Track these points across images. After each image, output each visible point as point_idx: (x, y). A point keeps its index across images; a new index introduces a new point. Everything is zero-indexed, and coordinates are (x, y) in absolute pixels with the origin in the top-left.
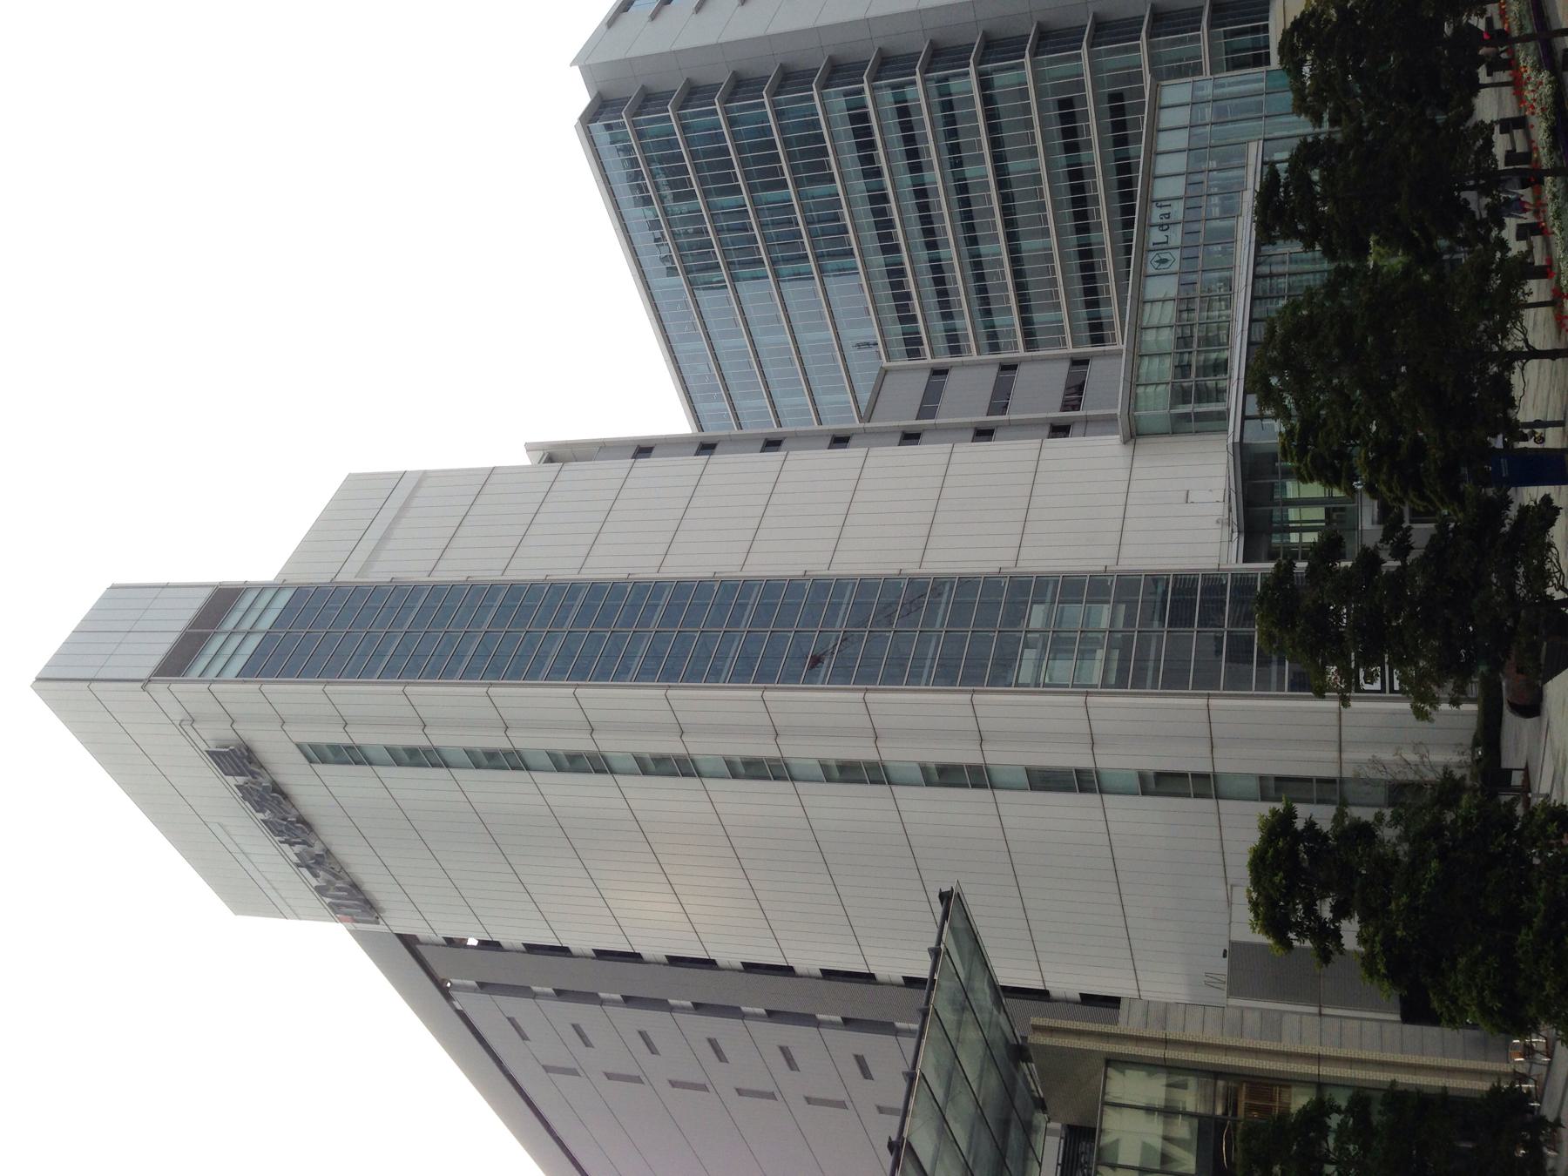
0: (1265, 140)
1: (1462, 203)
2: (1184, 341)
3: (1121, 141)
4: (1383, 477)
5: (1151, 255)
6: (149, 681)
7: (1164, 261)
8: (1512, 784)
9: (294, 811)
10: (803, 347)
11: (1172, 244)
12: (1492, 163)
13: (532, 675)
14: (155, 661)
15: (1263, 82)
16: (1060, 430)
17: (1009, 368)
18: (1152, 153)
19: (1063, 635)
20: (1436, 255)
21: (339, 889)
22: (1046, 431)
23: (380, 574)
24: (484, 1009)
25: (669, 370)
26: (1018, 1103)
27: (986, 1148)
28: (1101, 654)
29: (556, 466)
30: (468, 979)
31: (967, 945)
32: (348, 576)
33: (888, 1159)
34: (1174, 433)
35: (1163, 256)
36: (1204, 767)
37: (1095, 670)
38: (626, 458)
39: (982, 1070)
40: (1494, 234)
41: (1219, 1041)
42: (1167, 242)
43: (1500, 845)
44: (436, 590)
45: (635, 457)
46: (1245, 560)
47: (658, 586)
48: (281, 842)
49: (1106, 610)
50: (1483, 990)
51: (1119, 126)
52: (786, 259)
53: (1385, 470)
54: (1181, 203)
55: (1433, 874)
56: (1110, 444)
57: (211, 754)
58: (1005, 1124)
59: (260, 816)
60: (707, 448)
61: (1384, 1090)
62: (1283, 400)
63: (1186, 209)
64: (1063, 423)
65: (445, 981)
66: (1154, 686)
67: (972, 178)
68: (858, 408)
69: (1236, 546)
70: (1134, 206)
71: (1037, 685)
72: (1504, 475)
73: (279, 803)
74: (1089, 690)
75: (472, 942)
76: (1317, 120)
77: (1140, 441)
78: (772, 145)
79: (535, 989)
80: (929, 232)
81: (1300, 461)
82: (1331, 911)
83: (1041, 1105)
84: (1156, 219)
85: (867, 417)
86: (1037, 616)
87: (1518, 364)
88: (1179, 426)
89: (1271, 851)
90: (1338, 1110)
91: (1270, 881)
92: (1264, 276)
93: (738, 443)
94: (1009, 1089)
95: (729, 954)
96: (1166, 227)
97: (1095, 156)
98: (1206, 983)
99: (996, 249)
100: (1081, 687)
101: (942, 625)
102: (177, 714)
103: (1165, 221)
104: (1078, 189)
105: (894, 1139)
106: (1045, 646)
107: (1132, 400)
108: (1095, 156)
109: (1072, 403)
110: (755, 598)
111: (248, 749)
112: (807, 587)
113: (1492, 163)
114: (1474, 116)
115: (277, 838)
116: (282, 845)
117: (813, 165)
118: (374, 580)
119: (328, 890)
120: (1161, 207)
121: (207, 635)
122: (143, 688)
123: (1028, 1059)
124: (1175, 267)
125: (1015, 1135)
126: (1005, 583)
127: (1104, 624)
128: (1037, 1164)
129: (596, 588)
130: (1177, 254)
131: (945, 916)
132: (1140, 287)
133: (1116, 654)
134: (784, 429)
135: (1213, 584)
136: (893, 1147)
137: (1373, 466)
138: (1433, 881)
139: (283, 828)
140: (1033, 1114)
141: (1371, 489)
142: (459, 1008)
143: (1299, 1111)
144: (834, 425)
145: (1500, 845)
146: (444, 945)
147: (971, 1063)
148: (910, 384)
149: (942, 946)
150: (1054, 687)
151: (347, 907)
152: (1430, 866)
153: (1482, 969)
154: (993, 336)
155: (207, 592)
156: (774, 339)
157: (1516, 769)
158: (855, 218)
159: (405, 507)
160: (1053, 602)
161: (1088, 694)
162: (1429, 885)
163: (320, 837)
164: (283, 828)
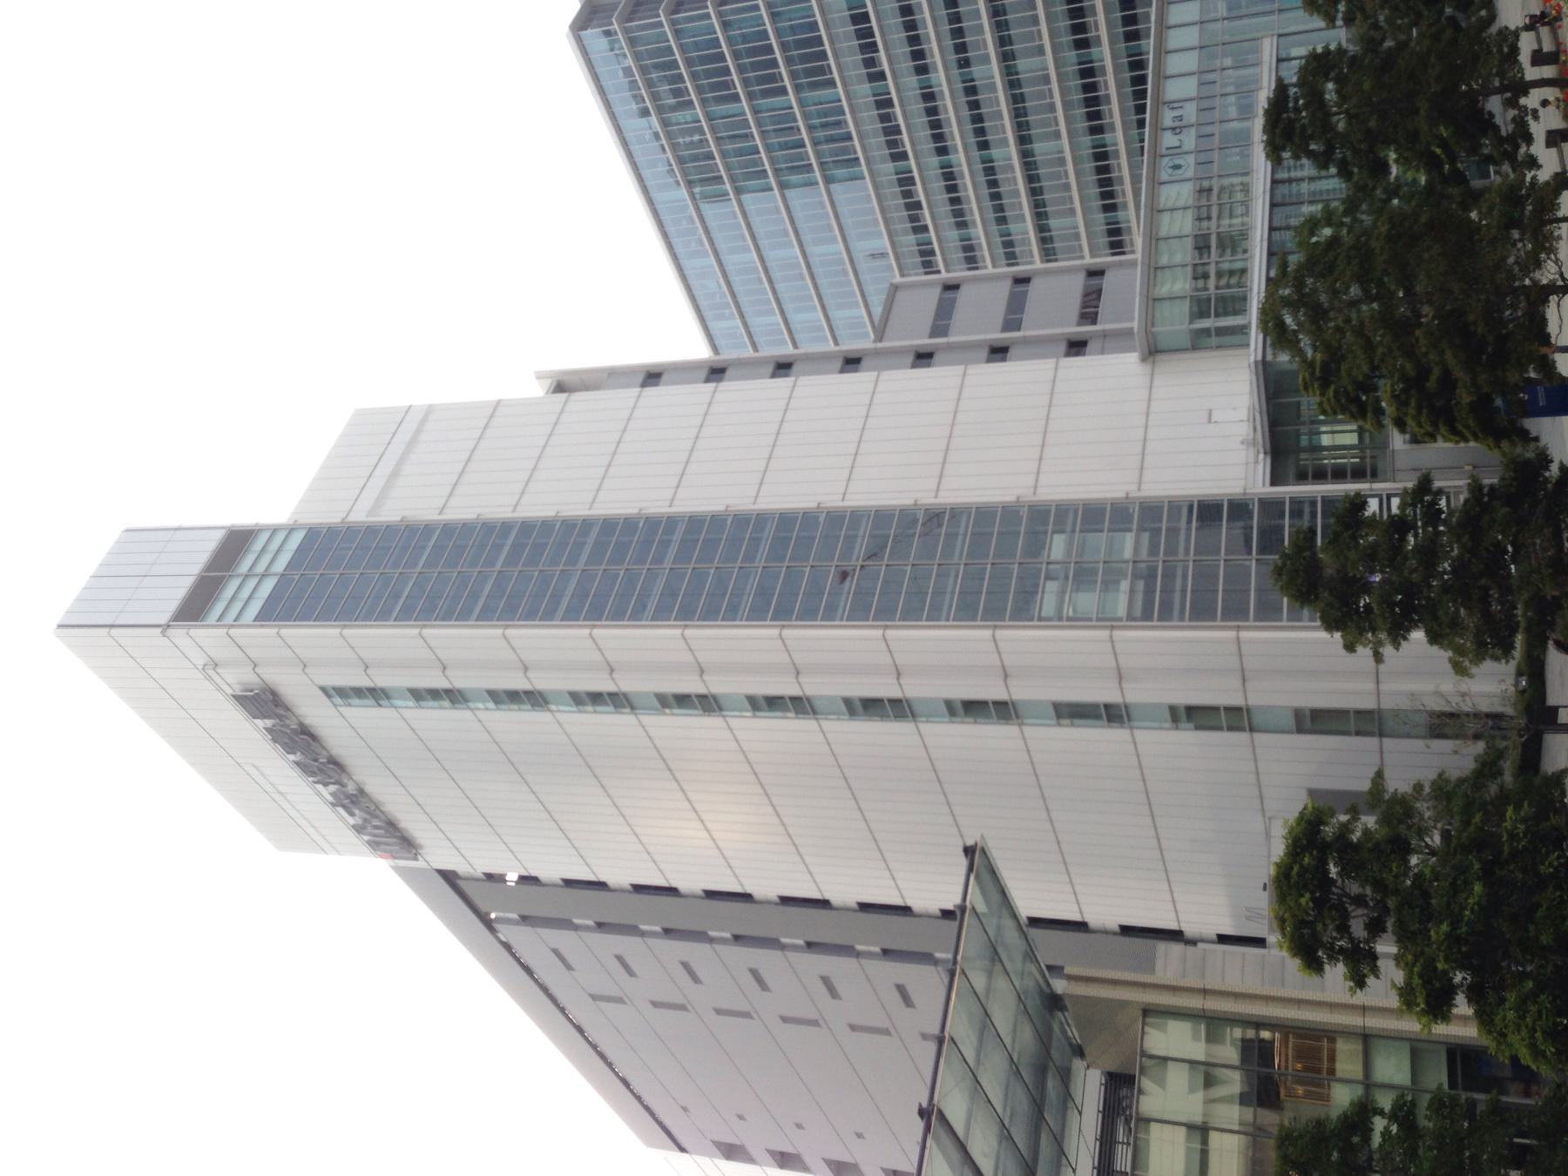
0: (1280, 36)
1: (1486, 117)
2: (1202, 245)
3: (1132, 36)
4: (1412, 411)
5: (1166, 160)
6: (169, 626)
8: (1559, 722)
9: (324, 753)
10: (813, 261)
11: (1186, 148)
12: (1518, 72)
13: (549, 615)
14: (173, 606)
16: (1077, 347)
17: (1022, 281)
18: (1162, 52)
19: (1084, 565)
20: (1459, 178)
21: (376, 827)
22: (1063, 347)
23: (391, 513)
24: (527, 941)
26: (1055, 1054)
27: (1023, 1104)
28: (1125, 585)
29: (563, 396)
30: (510, 912)
31: (995, 897)
32: (360, 516)
33: (920, 1125)
34: (1195, 347)
35: (1177, 162)
36: (1236, 700)
37: (1120, 602)
38: (635, 386)
39: (1015, 1024)
40: (1523, 150)
41: (1259, 991)
42: (1180, 147)
43: (1551, 865)
44: (448, 529)
45: (644, 385)
46: (1273, 483)
47: (671, 522)
48: (315, 783)
49: (1129, 538)
50: (1535, 1031)
52: (792, 170)
53: (1413, 405)
54: (1195, 103)
55: (1477, 899)
56: (1128, 363)
57: (234, 696)
58: (1041, 1070)
59: (292, 757)
60: (716, 372)
61: (1432, 1092)
62: (1298, 341)
63: (1200, 110)
64: (1082, 338)
65: (488, 914)
66: (1182, 619)
67: (981, 79)
68: (872, 322)
69: (1263, 467)
71: (1060, 619)
72: (1541, 404)
73: (309, 745)
74: (1114, 623)
75: (512, 877)
76: (1331, 20)
77: (1159, 357)
78: (769, 50)
79: (576, 921)
80: (938, 138)
81: (1322, 394)
82: (1365, 929)
83: (1079, 1052)
85: (880, 337)
86: (1058, 547)
87: (1553, 299)
88: (1199, 342)
89: (1296, 868)
90: (1381, 1113)
91: (1296, 901)
92: (1283, 182)
93: (748, 368)
94: (1044, 1040)
95: (765, 887)
96: (1178, 131)
97: (1105, 54)
98: (1247, 918)
99: (1008, 153)
100: (1105, 620)
101: (960, 558)
102: (200, 661)
103: (1177, 124)
104: (1090, 88)
105: (925, 1105)
106: (1067, 577)
107: (1149, 320)
108: (1105, 54)
109: (1089, 314)
110: (769, 532)
111: (274, 694)
112: (822, 520)
113: (1518, 72)
114: (1497, 20)
115: (311, 779)
116: (316, 785)
117: (813, 68)
118: (384, 519)
119: (365, 828)
120: (1173, 109)
121: (224, 577)
123: (1063, 1008)
124: (1190, 173)
125: (1052, 1083)
126: (1024, 513)
127: (1128, 553)
128: (1076, 1111)
129: (609, 525)
130: (1191, 159)
131: (971, 869)
132: (1153, 195)
133: (1141, 585)
134: (801, 351)
135: (1239, 508)
136: (924, 1113)
137: (1400, 400)
138: (1476, 907)
139: (315, 769)
140: (1071, 1061)
141: (1401, 425)
142: (504, 939)
143: (1339, 1118)
144: (851, 345)
145: (1551, 865)
146: (483, 880)
147: (1004, 1015)
148: (922, 302)
149: (968, 903)
150: (1079, 620)
151: (386, 844)
152: (1473, 889)
153: (1533, 1008)
154: (1008, 244)
155: (218, 536)
156: (784, 254)
157: (1563, 707)
158: (860, 124)
159: (413, 442)
160: (1073, 531)
161: (1112, 628)
162: (1472, 911)
163: (354, 777)
164: (315, 769)
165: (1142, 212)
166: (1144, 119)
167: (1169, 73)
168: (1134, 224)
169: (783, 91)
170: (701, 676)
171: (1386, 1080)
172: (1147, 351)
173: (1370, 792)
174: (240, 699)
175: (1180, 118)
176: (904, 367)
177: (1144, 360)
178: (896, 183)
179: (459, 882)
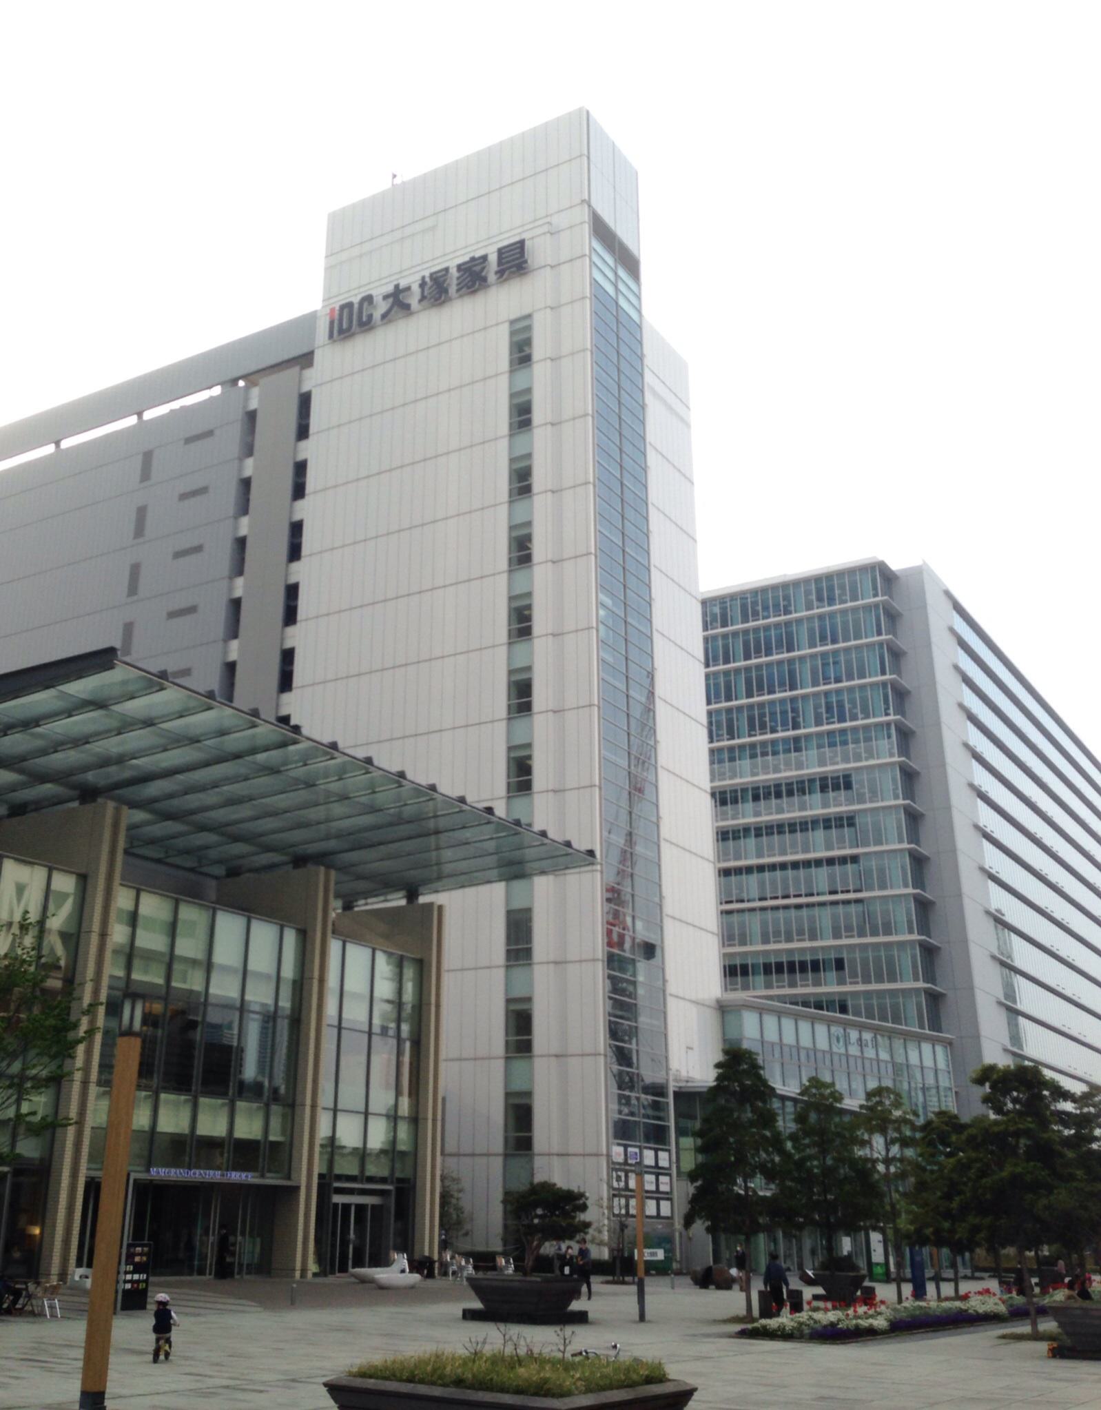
14: (600, 211)
25: (718, 590)
46: (675, 1093)
51: (779, 968)
70: (874, 1019)
103: (864, 1042)
122: (583, 201)
132: (771, 1011)
165: (764, 1001)
166: (810, 1007)
167: (349, 947)
168: (752, 993)
169: (750, 695)
170: (552, 634)
171: (57, 1135)
172: (724, 1004)
174: (521, 243)
175: (866, 1045)
177: (718, 1001)
178: (767, 801)
179: (297, 369)
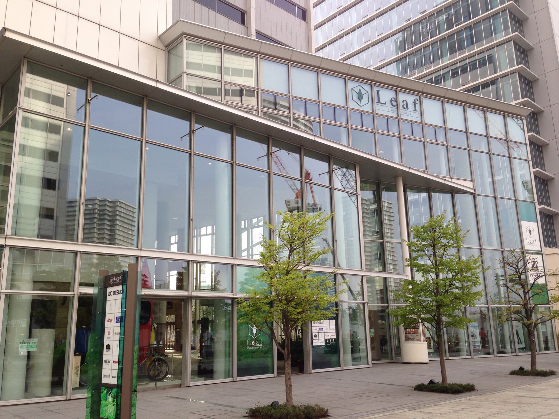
7: (360, 97)
15: (180, 287)
42: (379, 102)
84: (402, 97)
96: (394, 103)
103: (401, 104)
120: (415, 103)
124: (352, 105)
130: (368, 108)
173: (263, 240)
176: (203, 380)
